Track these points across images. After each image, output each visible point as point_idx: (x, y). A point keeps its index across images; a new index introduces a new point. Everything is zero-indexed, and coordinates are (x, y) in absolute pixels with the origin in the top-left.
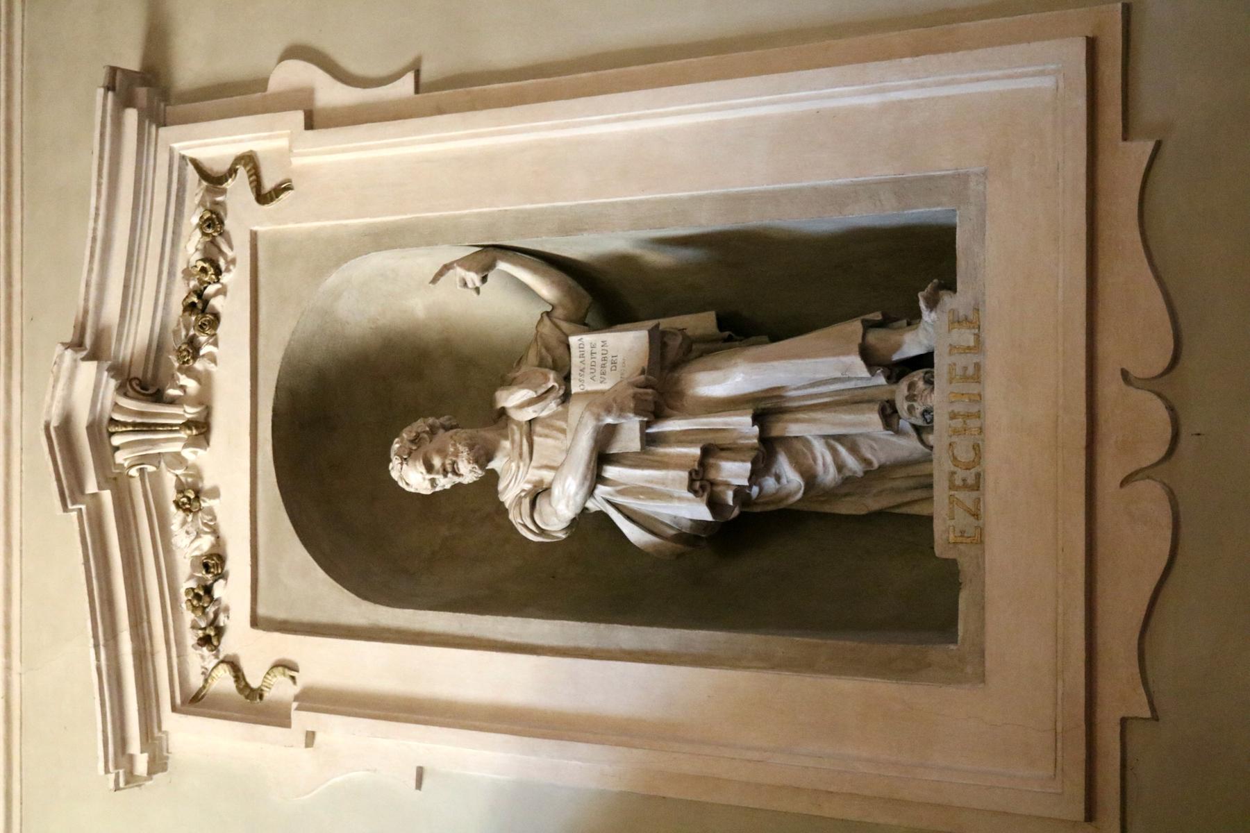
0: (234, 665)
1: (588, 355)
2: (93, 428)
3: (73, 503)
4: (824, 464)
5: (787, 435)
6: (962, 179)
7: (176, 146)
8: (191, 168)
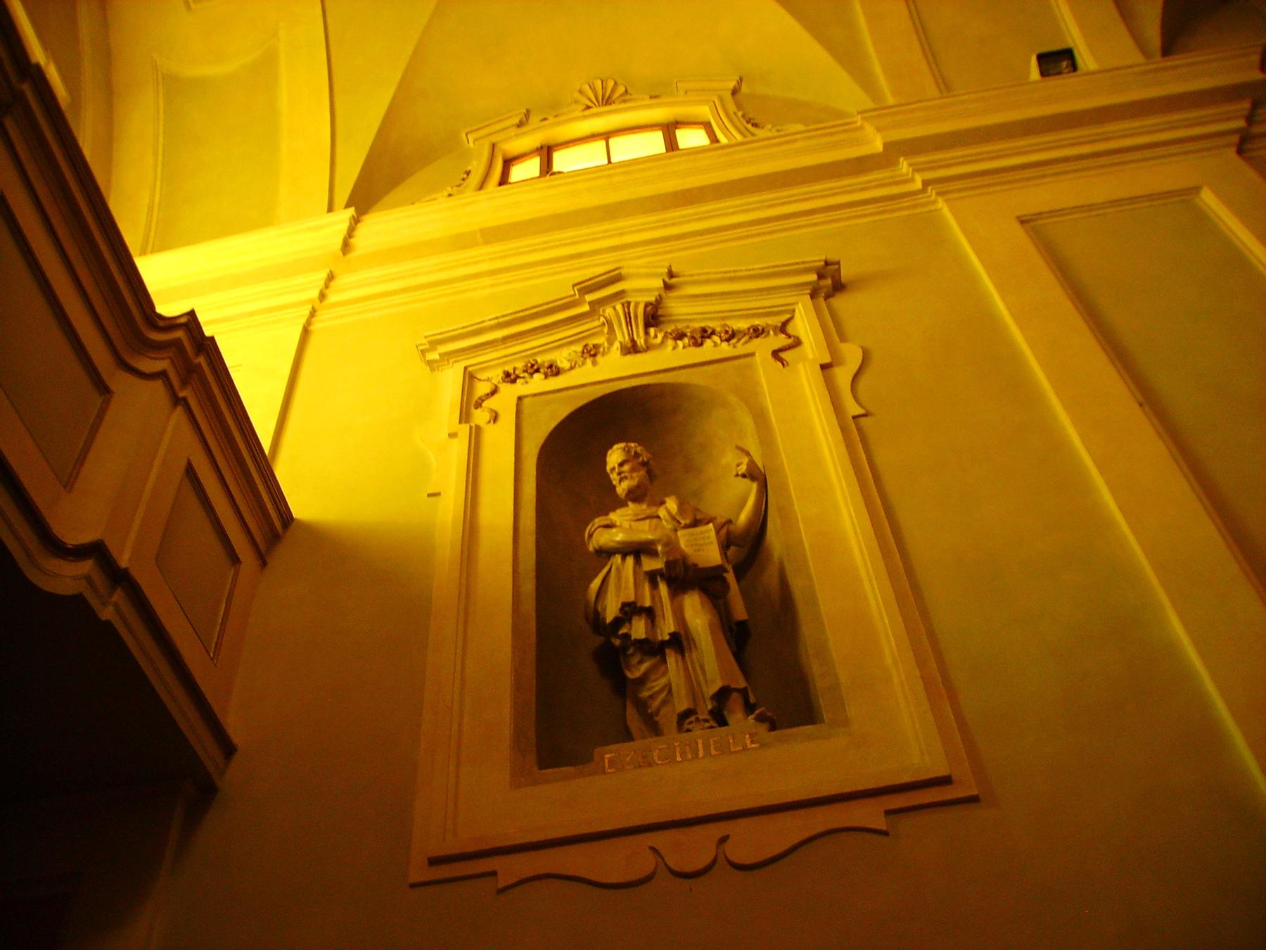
0: (494, 392)
1: (702, 536)
2: (621, 293)
3: (578, 290)
4: (653, 687)
5: (667, 658)
6: (846, 723)
7: (800, 305)
8: (788, 316)
